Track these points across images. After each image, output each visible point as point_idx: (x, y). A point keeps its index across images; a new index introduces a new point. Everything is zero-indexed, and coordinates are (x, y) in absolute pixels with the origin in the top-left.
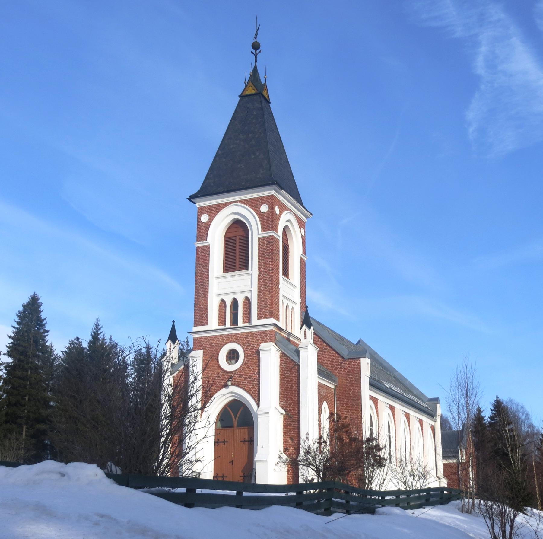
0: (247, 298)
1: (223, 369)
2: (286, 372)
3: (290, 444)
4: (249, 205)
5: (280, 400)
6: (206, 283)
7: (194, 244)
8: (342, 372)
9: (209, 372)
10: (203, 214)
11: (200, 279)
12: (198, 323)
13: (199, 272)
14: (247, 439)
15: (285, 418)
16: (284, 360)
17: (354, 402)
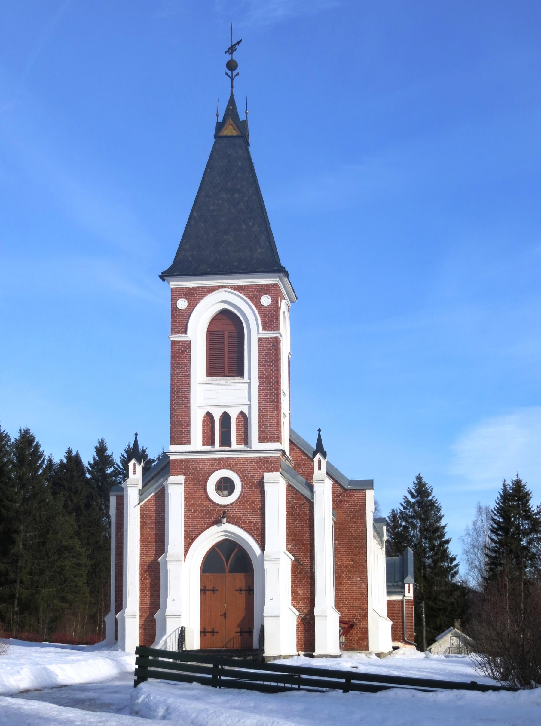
0: (242, 413)
1: (213, 501)
2: (294, 508)
3: (300, 596)
4: (244, 294)
5: (286, 543)
6: (187, 390)
7: (168, 337)
8: (342, 505)
10: (180, 298)
11: (178, 384)
13: (176, 375)
15: (294, 565)
16: (292, 494)
17: (357, 542)
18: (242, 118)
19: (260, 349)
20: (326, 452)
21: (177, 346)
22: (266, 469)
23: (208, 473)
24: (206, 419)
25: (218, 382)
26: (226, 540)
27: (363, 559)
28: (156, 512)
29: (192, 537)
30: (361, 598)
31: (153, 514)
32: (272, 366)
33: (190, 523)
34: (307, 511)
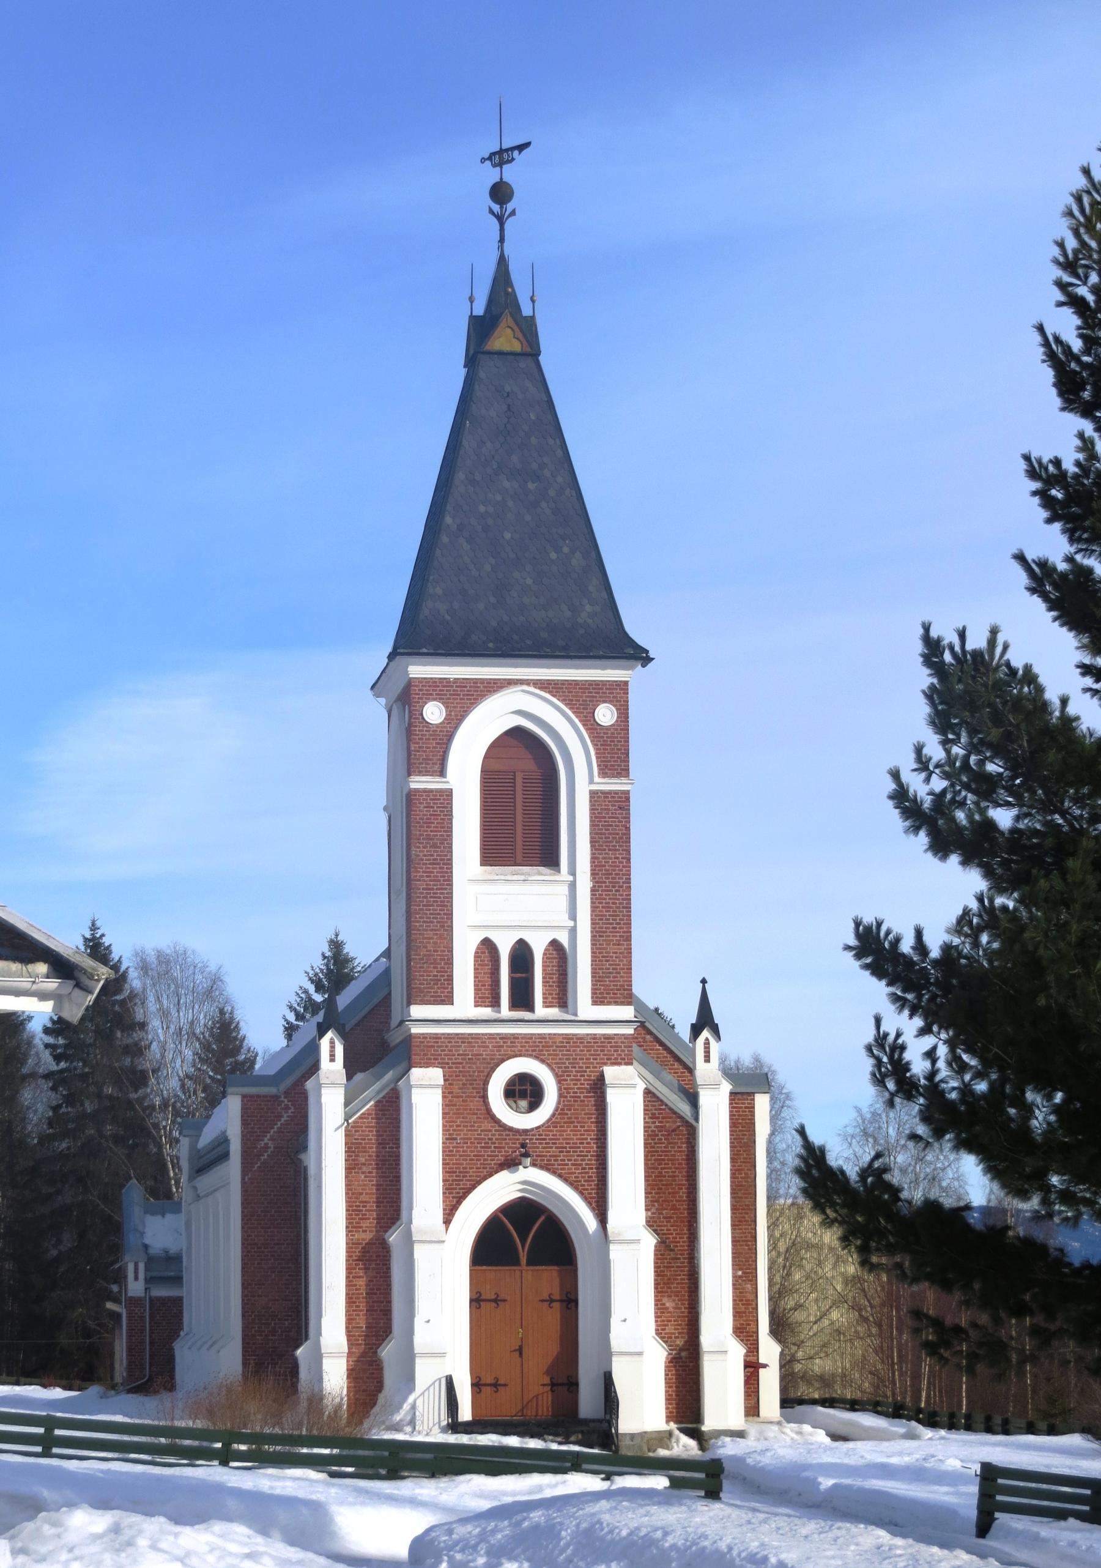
0: (555, 944)
9: (459, 1126)
11: (426, 879)
12: (424, 996)
13: (422, 860)
14: (557, 1296)
18: (526, 311)
19: (594, 813)
20: (717, 1025)
21: (424, 799)
22: (607, 1059)
23: (489, 1063)
24: (482, 953)
25: (509, 877)
26: (522, 1200)
27: (749, 1233)
28: (377, 1140)
29: (458, 1193)
30: (745, 1312)
31: (372, 1144)
32: (618, 850)
33: (453, 1164)
34: (682, 1143)
